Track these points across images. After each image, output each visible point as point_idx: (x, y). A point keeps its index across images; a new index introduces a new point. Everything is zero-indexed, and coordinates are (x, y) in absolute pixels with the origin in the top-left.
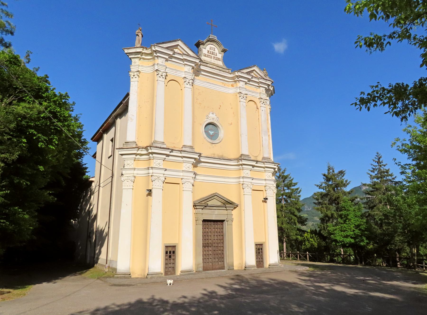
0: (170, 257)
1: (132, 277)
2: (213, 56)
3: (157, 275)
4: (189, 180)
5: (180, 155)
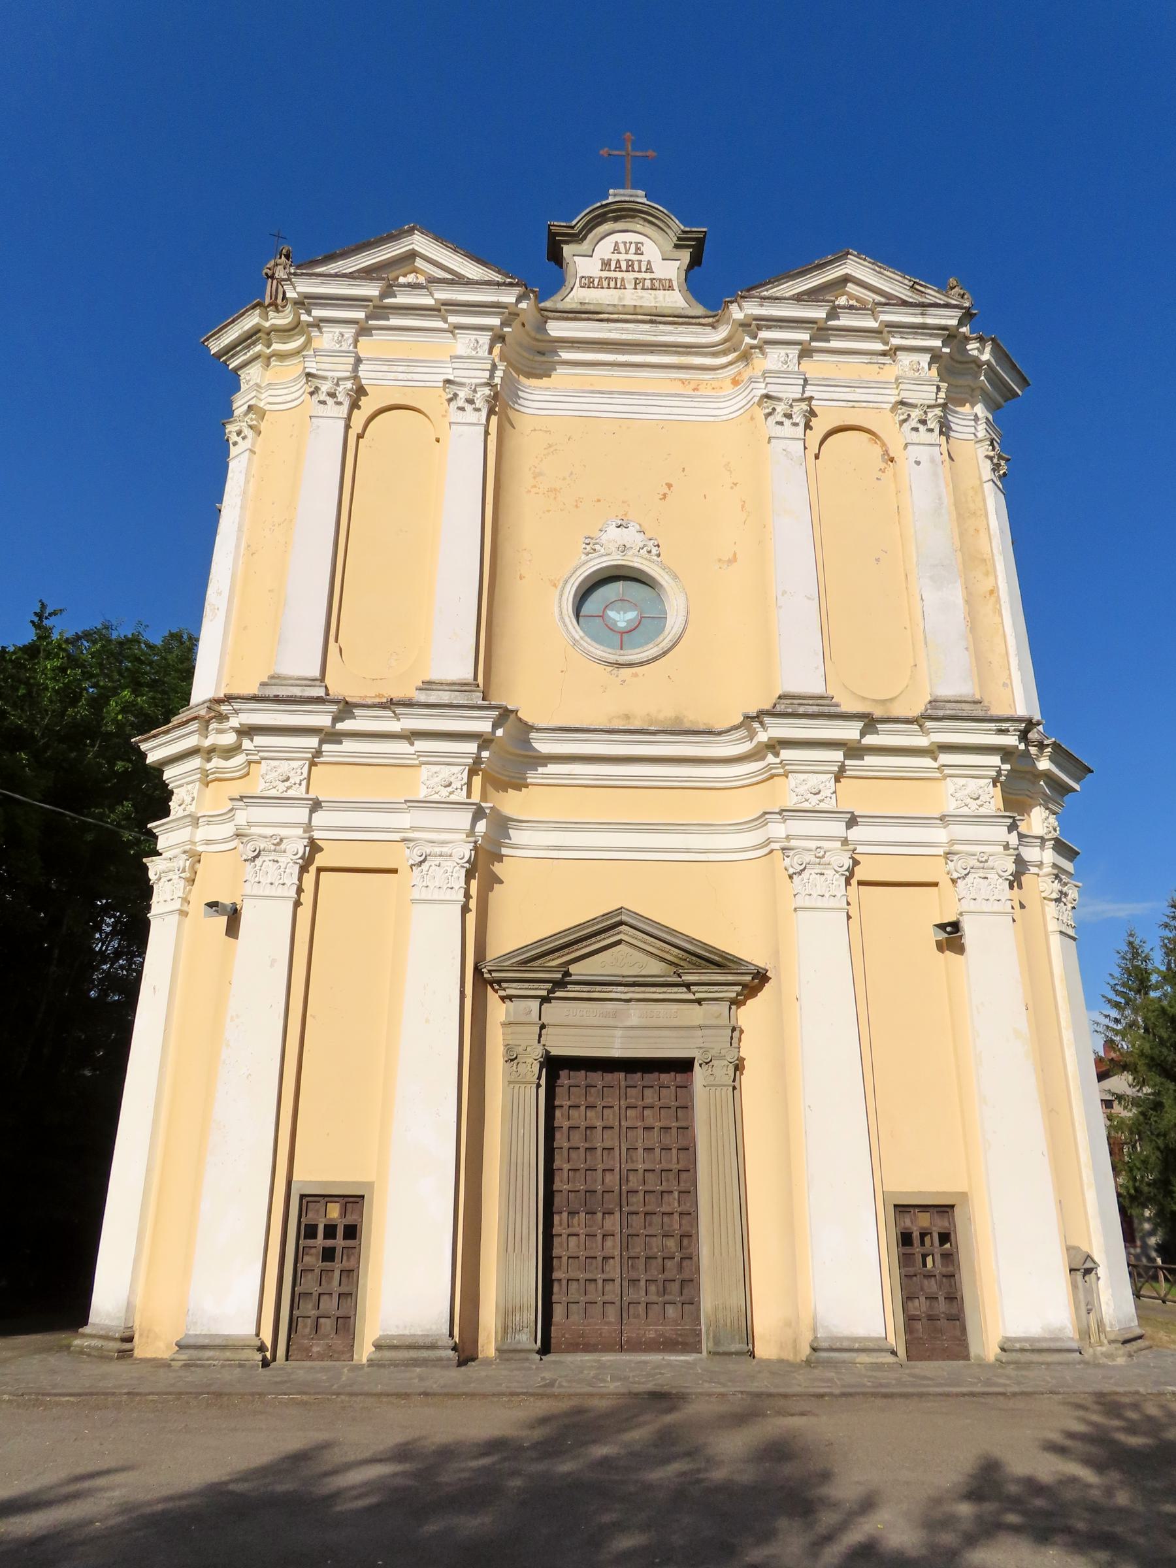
0: (328, 1255)
1: (138, 1353)
2: (630, 276)
3: (228, 1354)
4: (445, 850)
5: (395, 726)
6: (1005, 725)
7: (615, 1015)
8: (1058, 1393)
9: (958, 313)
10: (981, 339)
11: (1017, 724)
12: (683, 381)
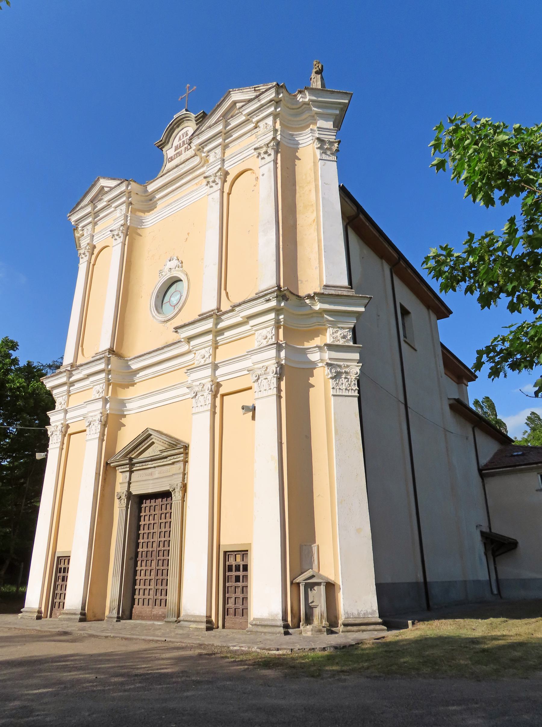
6: (267, 297)
7: (151, 474)
8: (122, 638)
9: (273, 90)
10: (300, 92)
11: (273, 295)
12: (196, 184)
